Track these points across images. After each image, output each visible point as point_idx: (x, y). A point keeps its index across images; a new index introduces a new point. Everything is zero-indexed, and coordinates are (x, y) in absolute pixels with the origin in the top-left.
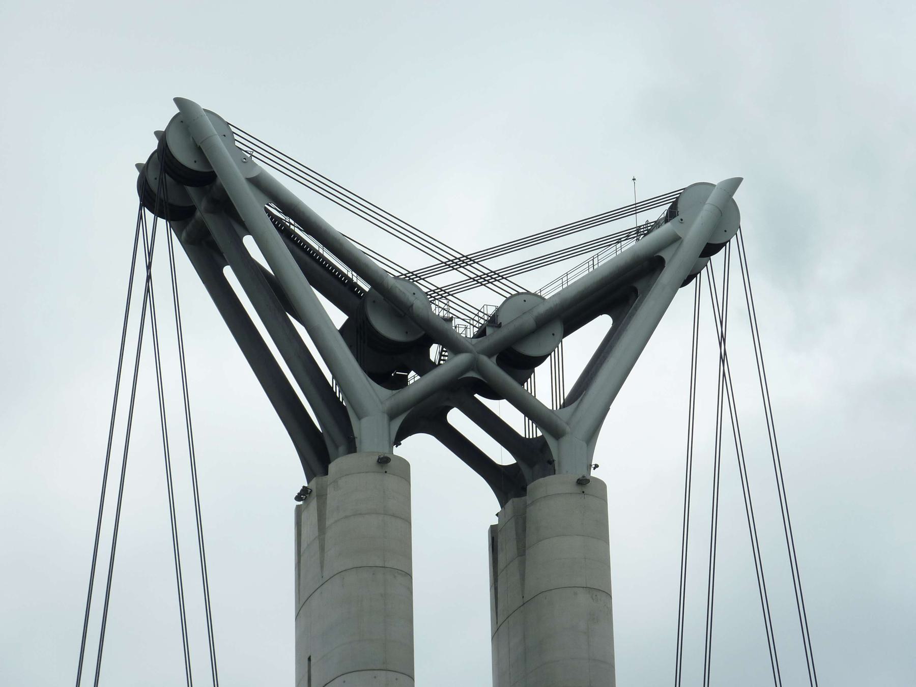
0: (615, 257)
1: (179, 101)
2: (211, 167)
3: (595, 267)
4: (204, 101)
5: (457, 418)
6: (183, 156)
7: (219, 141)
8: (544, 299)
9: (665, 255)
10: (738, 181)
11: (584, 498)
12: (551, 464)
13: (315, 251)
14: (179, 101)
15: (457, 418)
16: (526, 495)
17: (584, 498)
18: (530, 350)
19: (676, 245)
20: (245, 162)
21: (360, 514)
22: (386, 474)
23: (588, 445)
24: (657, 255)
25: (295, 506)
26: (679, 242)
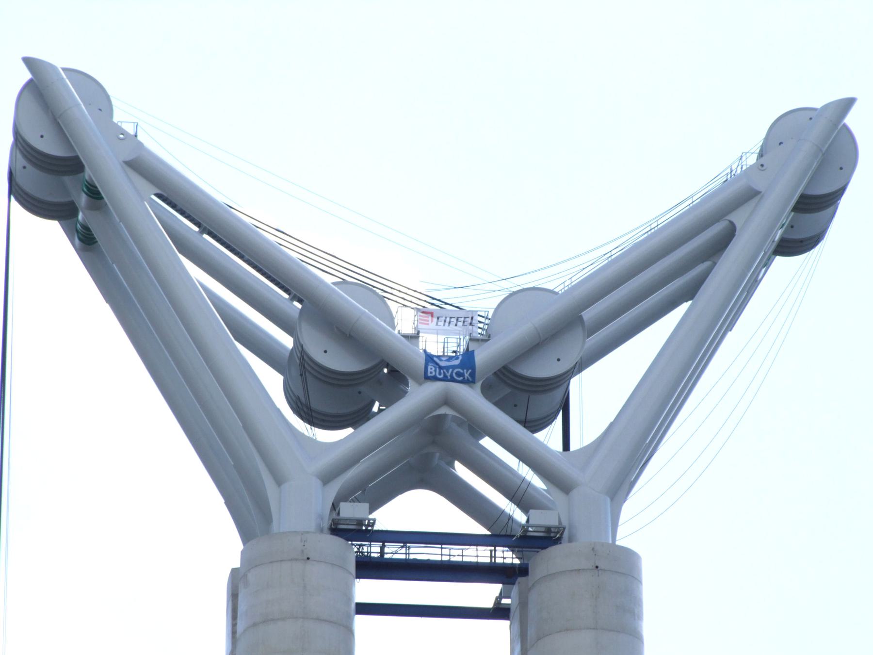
0: (607, 263)
1: (29, 62)
2: (74, 151)
3: (744, 169)
5: (461, 470)
6: (50, 146)
8: (557, 293)
9: (738, 218)
10: (848, 104)
11: (598, 576)
12: (557, 541)
13: (664, 425)
14: (29, 62)
15: (461, 470)
16: (513, 584)
17: (598, 576)
19: (755, 200)
20: (122, 139)
21: (273, 620)
22: (308, 561)
23: (612, 499)
24: (409, 378)
25: (231, 569)
26: (759, 197)
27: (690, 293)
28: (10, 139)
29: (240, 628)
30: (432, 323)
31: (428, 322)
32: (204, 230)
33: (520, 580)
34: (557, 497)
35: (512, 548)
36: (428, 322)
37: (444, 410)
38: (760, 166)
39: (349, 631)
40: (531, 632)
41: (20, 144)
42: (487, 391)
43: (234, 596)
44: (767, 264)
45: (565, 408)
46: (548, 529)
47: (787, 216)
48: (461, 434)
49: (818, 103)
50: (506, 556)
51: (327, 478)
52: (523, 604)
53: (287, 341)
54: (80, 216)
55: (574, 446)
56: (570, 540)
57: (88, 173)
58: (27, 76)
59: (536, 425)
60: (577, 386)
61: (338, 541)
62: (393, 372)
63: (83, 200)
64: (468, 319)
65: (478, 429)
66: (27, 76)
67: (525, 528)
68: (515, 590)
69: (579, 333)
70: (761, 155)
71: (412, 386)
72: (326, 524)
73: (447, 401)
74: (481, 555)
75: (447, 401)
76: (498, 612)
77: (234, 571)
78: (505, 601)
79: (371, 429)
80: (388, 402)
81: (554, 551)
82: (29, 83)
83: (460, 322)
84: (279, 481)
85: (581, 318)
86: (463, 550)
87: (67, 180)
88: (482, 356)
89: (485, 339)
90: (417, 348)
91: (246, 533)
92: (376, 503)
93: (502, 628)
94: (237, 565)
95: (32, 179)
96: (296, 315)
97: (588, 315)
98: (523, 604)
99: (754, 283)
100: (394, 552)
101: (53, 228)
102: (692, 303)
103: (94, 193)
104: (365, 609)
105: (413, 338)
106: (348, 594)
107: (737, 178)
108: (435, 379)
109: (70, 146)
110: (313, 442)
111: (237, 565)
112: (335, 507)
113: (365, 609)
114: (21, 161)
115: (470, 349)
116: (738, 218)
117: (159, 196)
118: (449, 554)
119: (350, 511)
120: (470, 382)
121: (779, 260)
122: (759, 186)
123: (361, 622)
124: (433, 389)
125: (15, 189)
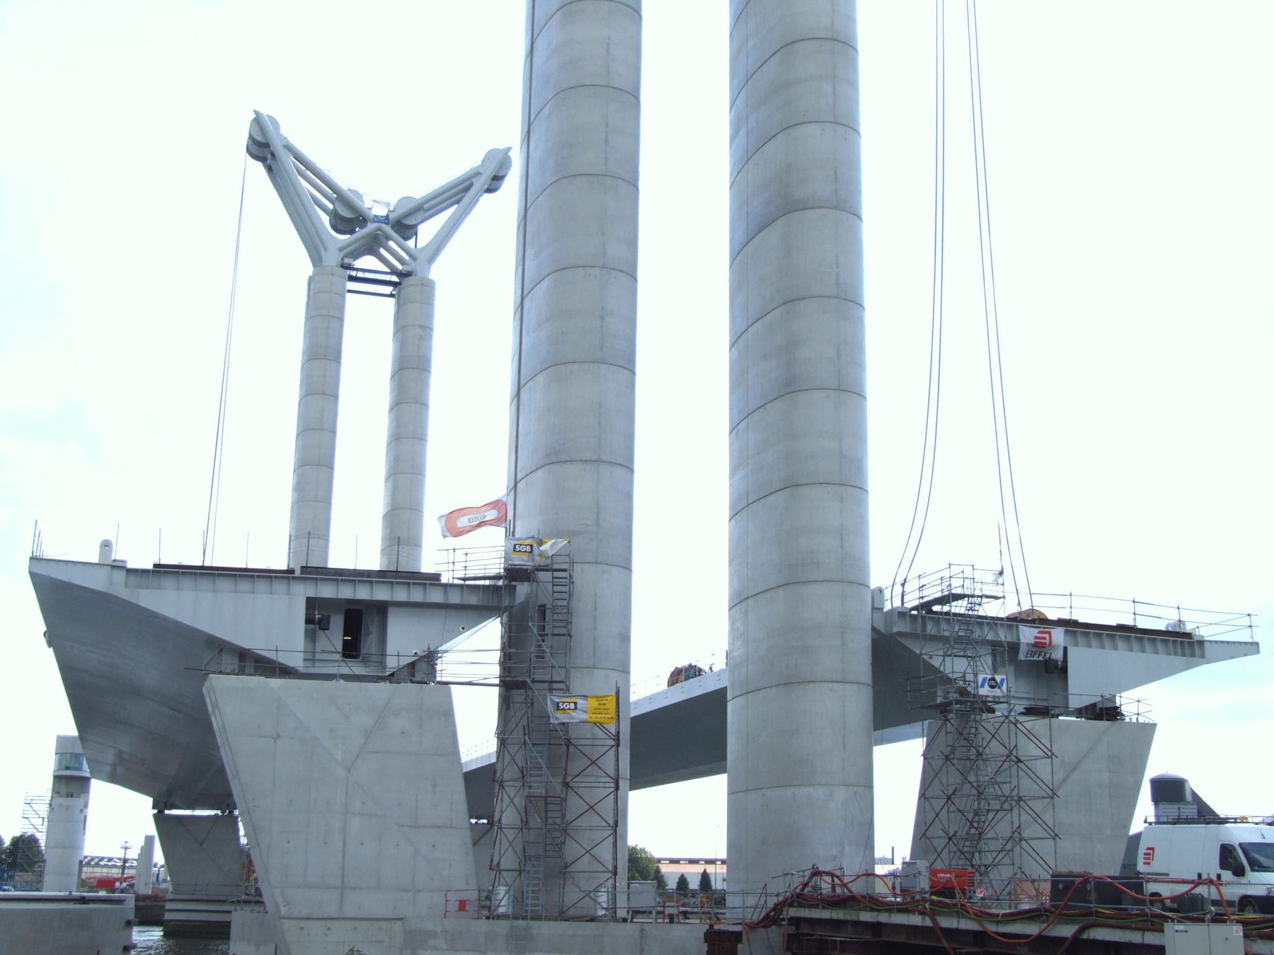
4: (265, 111)
5: (382, 251)
6: (260, 138)
7: (271, 128)
9: (474, 180)
14: (254, 111)
15: (382, 251)
18: (409, 222)
27: (458, 202)
28: (248, 136)
29: (311, 294)
30: (376, 204)
31: (1148, 861)
32: (307, 169)
33: (399, 286)
34: (412, 262)
35: (397, 276)
36: (1148, 861)
37: (379, 232)
38: (482, 165)
39: (343, 297)
40: (401, 303)
41: (251, 138)
42: (392, 227)
43: (309, 284)
44: (481, 195)
45: (416, 234)
46: (408, 272)
47: (489, 181)
48: (383, 240)
49: (501, 148)
50: (395, 279)
51: (341, 250)
52: (399, 293)
53: (331, 206)
54: (268, 162)
55: (418, 247)
56: (415, 275)
57: (272, 148)
58: (255, 116)
59: (406, 239)
60: (421, 228)
61: (342, 269)
62: (363, 219)
63: (269, 156)
64: (388, 205)
65: (388, 238)
66: (255, 116)
67: (401, 271)
68: (397, 289)
69: (422, 212)
70: (483, 162)
71: (369, 224)
72: (340, 264)
73: (379, 229)
74: (387, 278)
75: (379, 229)
76: (391, 295)
77: (310, 277)
78: (393, 292)
79: (355, 236)
80: (361, 228)
81: (410, 278)
82: (255, 119)
83: (1137, 719)
84: (326, 250)
85: (423, 208)
86: (565, 667)
87: (265, 149)
88: (392, 216)
89: (393, 211)
90: (1067, 942)
91: (315, 265)
92: (356, 257)
93: (392, 300)
94: (311, 274)
95: (255, 149)
96: (334, 199)
97: (426, 206)
98: (399, 293)
99: (478, 200)
100: (360, 274)
101: (259, 165)
102: (457, 208)
103: (273, 155)
104: (349, 291)
105: (370, 209)
106: (344, 286)
107: (475, 168)
108: (376, 222)
109: (266, 139)
110: (336, 238)
111: (311, 274)
112: (343, 259)
113: (349, 291)
114: (251, 143)
115: (1024, 711)
116: (474, 180)
117: (294, 158)
118: (589, 763)
119: (347, 261)
120: (387, 224)
121: (486, 195)
122: (481, 171)
123: (348, 295)
124: (375, 225)
125: (248, 151)
